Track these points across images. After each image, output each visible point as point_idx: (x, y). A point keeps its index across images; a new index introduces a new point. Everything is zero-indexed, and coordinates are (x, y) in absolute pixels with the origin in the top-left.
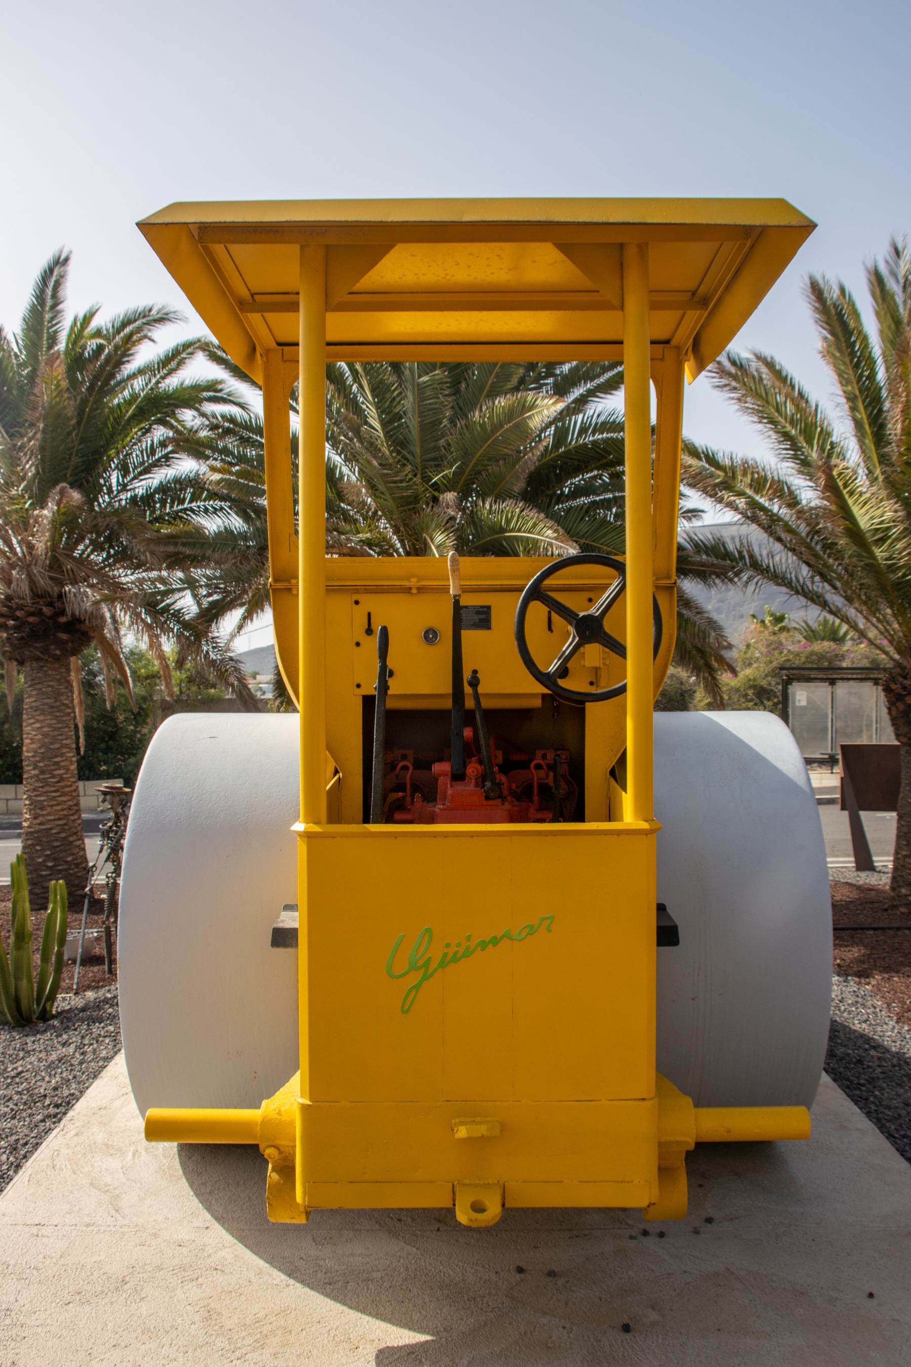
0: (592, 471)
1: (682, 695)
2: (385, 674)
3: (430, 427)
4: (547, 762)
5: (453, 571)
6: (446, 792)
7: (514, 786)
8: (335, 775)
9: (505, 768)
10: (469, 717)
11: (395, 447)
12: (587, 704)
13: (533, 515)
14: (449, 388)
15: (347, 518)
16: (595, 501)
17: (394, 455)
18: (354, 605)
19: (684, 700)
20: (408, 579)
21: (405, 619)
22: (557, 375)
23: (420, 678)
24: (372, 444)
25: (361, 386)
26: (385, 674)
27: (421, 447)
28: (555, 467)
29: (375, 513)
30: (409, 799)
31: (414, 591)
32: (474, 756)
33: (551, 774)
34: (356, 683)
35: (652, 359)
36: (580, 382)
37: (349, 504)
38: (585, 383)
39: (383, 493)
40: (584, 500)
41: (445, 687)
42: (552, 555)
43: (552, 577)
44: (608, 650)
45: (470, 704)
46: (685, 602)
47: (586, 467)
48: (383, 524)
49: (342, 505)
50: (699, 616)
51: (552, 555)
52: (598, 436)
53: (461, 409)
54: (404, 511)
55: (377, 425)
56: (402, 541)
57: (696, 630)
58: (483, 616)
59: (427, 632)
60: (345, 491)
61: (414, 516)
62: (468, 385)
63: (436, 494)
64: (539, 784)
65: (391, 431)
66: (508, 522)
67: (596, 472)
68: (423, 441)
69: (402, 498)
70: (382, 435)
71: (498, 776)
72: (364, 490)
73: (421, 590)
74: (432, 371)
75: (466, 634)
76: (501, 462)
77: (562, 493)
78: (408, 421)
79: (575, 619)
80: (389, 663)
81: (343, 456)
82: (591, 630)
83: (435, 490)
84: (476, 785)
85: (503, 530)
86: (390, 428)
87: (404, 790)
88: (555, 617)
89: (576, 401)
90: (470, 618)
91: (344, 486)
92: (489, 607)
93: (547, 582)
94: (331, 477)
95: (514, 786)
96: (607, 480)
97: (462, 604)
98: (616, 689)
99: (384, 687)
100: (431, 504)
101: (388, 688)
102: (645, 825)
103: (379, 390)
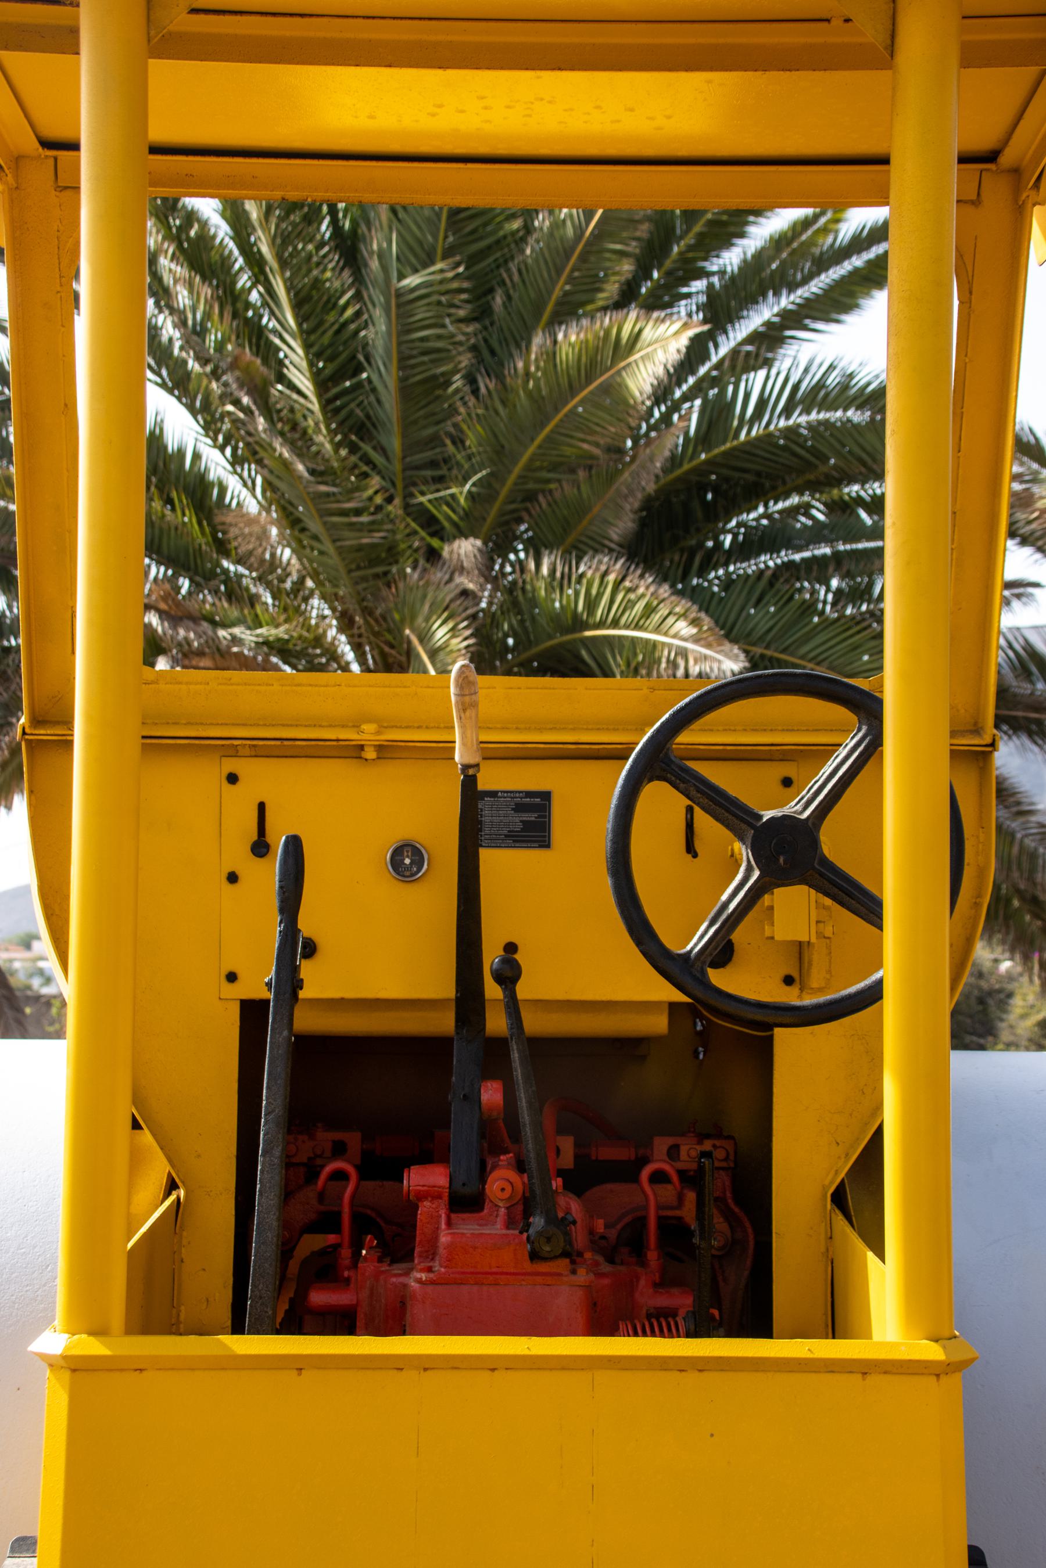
0: (786, 496)
1: (981, 1001)
2: (295, 949)
3: (422, 391)
4: (680, 1165)
5: (463, 708)
6: (436, 1238)
7: (600, 1225)
8: (168, 1194)
9: (578, 1180)
10: (494, 1055)
11: (345, 436)
12: (777, 1031)
13: (645, 587)
14: (467, 301)
15: (235, 592)
16: (792, 563)
17: (343, 452)
18: (226, 785)
19: (985, 1012)
20: (356, 726)
21: (348, 820)
22: (713, 274)
23: (382, 959)
24: (294, 426)
25: (270, 291)
26: (295, 949)
27: (404, 436)
28: (703, 488)
29: (301, 581)
30: (346, 1253)
31: (370, 754)
32: (505, 1151)
33: (691, 1196)
34: (226, 969)
35: (958, 201)
36: (764, 296)
37: (238, 561)
38: (777, 294)
39: (315, 538)
40: (768, 561)
41: (441, 984)
42: (687, 675)
43: (697, 725)
44: (828, 902)
45: (496, 1023)
46: (1005, 793)
47: (774, 488)
48: (317, 606)
49: (225, 564)
50: (1021, 819)
51: (687, 675)
52: (799, 418)
53: (493, 353)
54: (364, 579)
55: (304, 383)
56: (357, 648)
57: (1015, 850)
58: (531, 817)
59: (398, 853)
60: (233, 532)
61: (384, 592)
62: (509, 298)
63: (435, 543)
64: (662, 1221)
65: (336, 397)
66: (591, 604)
67: (795, 500)
68: (407, 424)
69: (360, 548)
70: (316, 407)
71: (562, 1201)
72: (274, 531)
73: (386, 751)
74: (425, 266)
75: (490, 859)
76: (582, 474)
77: (719, 545)
78: (375, 378)
79: (751, 826)
80: (306, 925)
81: (228, 451)
82: (790, 853)
83: (433, 535)
84: (509, 1223)
85: (579, 624)
86: (335, 391)
87: (337, 1229)
88: (703, 820)
89: (754, 338)
90: (500, 819)
91: (229, 519)
92: (546, 796)
93: (684, 738)
94: (167, 475)
95: (600, 1225)
96: (821, 517)
97: (481, 787)
98: (850, 997)
99: (289, 981)
100: (422, 562)
101: (298, 984)
102: (934, 1352)
103: (310, 304)
